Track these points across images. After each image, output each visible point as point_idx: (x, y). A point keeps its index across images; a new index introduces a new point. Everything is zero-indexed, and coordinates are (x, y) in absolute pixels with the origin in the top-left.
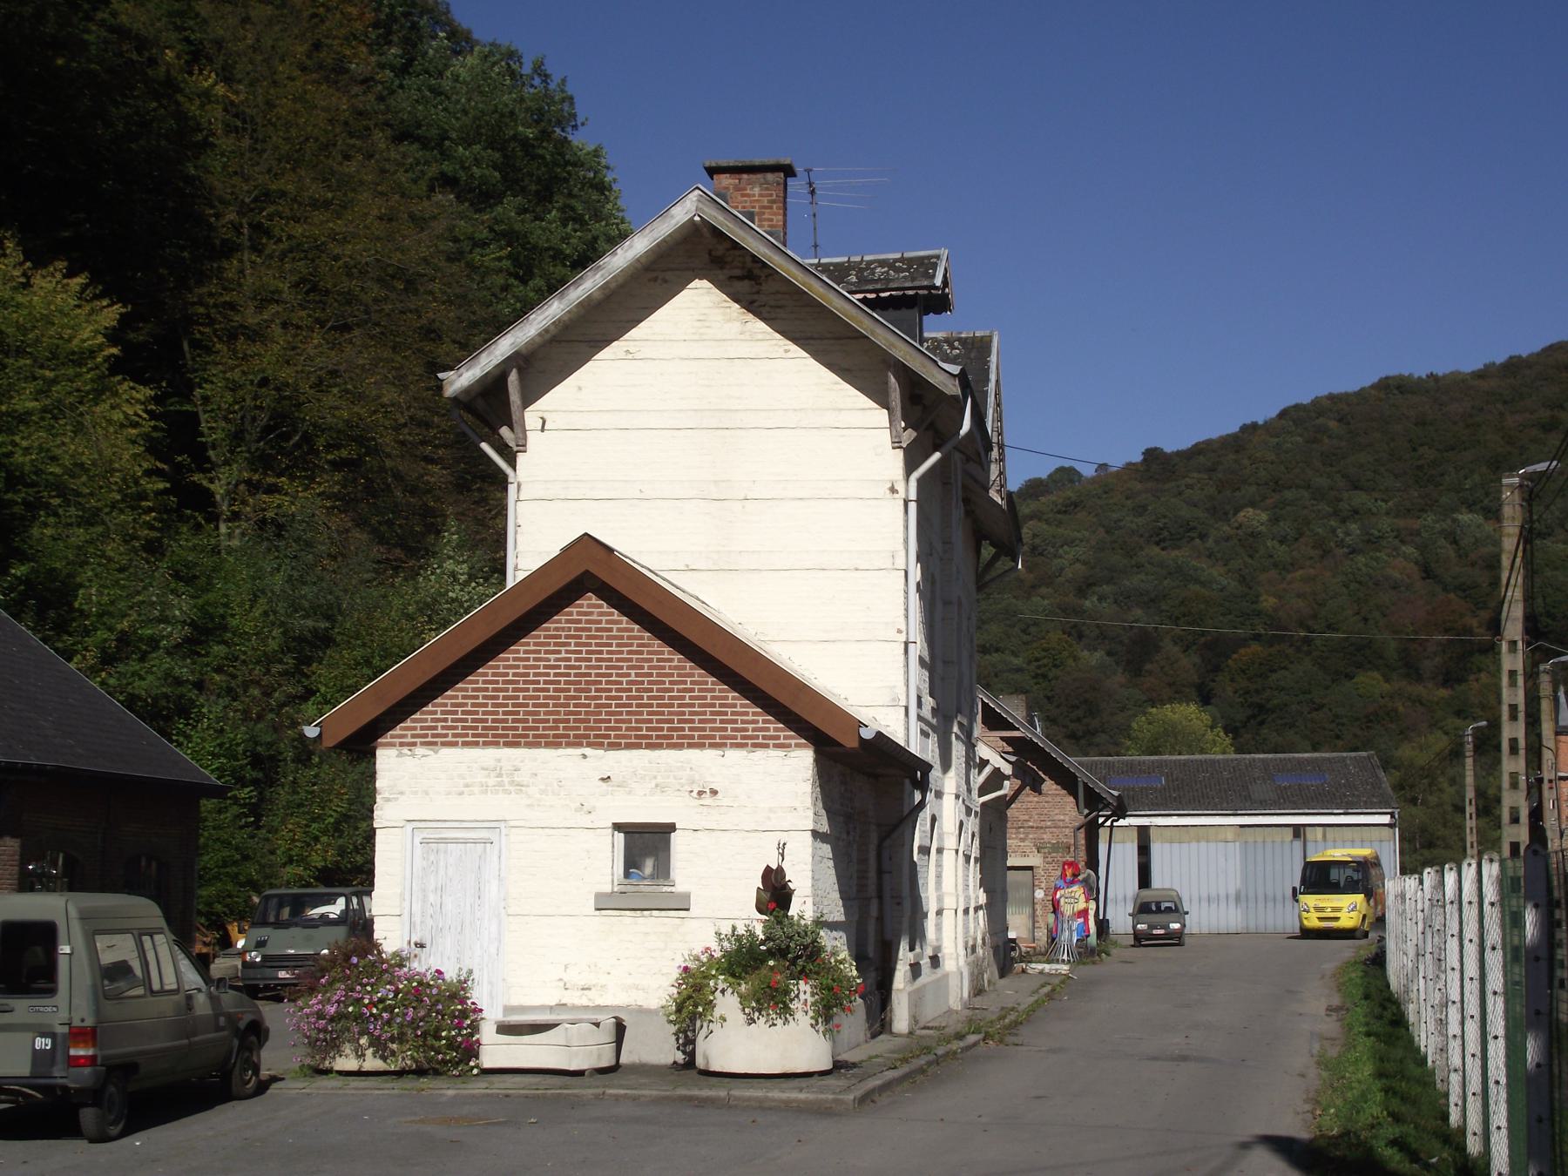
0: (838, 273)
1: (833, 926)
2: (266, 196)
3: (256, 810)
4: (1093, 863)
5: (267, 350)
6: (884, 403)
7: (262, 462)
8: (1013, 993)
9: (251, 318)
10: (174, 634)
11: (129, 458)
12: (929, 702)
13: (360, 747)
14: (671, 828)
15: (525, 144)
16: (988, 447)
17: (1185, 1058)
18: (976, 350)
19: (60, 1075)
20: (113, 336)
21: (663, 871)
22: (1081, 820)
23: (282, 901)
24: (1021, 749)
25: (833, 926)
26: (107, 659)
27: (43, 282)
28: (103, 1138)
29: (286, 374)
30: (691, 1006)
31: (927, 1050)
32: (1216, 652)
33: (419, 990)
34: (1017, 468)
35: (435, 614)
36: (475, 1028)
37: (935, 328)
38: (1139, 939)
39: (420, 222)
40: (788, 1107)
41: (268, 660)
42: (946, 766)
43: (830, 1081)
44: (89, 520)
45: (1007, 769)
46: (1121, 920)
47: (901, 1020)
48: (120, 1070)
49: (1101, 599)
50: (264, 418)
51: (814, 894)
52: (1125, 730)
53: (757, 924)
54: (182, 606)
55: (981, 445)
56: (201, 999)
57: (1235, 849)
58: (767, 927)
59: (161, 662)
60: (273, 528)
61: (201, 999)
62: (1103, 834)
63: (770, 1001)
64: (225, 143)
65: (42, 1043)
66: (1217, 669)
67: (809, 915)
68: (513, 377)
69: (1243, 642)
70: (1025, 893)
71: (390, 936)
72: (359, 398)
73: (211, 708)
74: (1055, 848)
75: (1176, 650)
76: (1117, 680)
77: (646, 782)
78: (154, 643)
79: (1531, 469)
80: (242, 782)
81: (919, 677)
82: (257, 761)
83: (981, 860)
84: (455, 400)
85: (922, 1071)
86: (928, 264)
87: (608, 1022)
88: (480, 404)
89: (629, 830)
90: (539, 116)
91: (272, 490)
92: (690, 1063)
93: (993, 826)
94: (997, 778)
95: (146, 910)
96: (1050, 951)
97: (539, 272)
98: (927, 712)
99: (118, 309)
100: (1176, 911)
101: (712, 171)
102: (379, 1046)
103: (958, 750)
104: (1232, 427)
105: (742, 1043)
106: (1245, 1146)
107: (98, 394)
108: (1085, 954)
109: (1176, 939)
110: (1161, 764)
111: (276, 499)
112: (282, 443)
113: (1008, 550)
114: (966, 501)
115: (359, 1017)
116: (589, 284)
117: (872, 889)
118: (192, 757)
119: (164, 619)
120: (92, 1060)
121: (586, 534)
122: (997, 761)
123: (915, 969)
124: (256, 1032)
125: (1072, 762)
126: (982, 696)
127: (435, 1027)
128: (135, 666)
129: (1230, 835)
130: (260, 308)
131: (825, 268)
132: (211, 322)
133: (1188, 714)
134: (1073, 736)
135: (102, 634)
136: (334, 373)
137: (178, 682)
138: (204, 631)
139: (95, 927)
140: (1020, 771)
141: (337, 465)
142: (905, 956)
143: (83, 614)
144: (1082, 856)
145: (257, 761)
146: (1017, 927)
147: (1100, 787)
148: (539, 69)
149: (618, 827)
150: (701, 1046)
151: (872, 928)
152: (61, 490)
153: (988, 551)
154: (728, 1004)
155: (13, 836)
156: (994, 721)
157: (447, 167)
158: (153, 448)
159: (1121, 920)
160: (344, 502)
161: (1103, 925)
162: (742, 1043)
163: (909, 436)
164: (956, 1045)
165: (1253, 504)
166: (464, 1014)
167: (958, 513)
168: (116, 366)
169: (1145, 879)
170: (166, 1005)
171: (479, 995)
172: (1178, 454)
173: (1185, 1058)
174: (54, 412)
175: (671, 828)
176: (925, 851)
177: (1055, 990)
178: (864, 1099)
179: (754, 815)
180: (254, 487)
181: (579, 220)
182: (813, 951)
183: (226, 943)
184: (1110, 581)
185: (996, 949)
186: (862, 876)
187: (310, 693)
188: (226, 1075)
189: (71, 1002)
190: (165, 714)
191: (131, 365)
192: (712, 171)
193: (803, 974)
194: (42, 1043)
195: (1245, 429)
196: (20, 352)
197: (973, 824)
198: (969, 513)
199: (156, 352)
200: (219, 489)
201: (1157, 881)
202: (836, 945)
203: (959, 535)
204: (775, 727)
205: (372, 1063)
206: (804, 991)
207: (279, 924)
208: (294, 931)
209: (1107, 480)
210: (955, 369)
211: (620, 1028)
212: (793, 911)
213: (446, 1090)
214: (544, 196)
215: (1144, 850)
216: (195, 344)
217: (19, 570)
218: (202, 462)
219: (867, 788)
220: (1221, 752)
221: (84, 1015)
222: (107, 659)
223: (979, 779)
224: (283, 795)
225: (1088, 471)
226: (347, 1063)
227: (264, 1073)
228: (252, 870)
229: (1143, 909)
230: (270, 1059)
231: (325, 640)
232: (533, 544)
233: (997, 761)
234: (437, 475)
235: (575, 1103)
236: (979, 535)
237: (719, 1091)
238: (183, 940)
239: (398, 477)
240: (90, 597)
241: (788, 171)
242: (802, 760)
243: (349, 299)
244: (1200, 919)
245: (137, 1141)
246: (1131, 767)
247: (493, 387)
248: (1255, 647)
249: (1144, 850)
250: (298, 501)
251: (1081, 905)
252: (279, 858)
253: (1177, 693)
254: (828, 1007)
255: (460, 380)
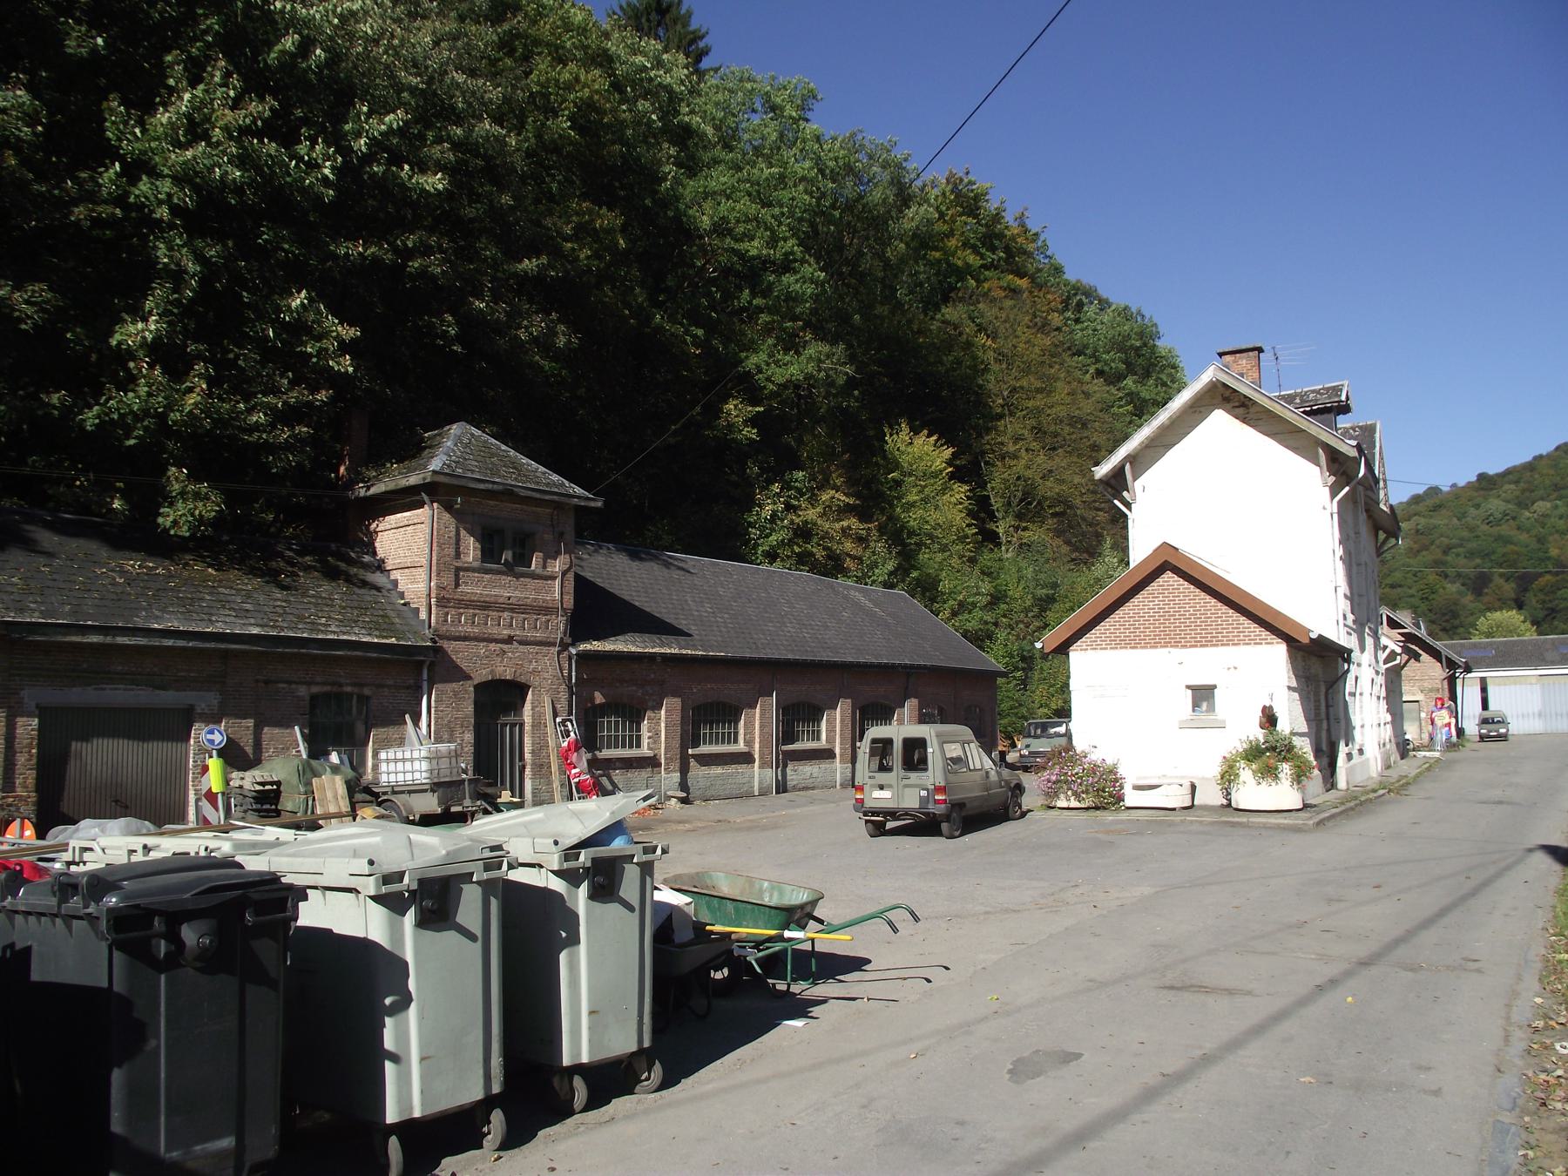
0: (1289, 399)
1: (1302, 735)
2: (1014, 390)
3: (1024, 683)
4: (1453, 697)
5: (1019, 461)
6: (1318, 465)
7: (1020, 516)
8: (1407, 768)
9: (1011, 448)
10: (985, 600)
11: (958, 518)
12: (1351, 617)
13: (1063, 649)
14: (1215, 687)
15: (1137, 349)
16: (1377, 481)
17: (1500, 802)
18: (1369, 431)
19: (932, 808)
20: (949, 463)
21: (1211, 709)
22: (1445, 675)
23: (1037, 726)
24: (1409, 638)
25: (1302, 735)
26: (954, 614)
27: (920, 440)
28: (952, 837)
29: (1028, 473)
30: (1228, 777)
31: (1356, 798)
32: (1525, 582)
33: (1094, 769)
34: (1395, 494)
35: (1099, 582)
36: (1122, 787)
37: (1343, 422)
38: (1482, 738)
39: (1087, 395)
40: (1279, 827)
41: (1026, 610)
42: (1363, 649)
43: (1300, 814)
44: (944, 548)
45: (1399, 650)
46: (1471, 728)
47: (1342, 782)
48: (958, 806)
49: (1458, 555)
50: (1019, 494)
51: (1292, 718)
52: (1474, 626)
53: (1259, 735)
54: (986, 587)
55: (1372, 482)
56: (993, 773)
57: (1538, 687)
58: (1265, 736)
59: (977, 613)
60: (1024, 547)
61: (993, 773)
62: (1459, 682)
63: (1269, 773)
64: (995, 367)
65: (924, 793)
66: (1526, 590)
67: (1287, 732)
68: (1128, 467)
69: (1541, 575)
70: (1415, 715)
71: (1079, 744)
72: (1063, 481)
73: (1001, 635)
74: (1431, 690)
75: (1501, 581)
76: (1468, 599)
77: (1203, 664)
78: (974, 605)
79: (596, 646)
80: (1017, 669)
81: (1345, 605)
82: (1023, 659)
83: (1387, 698)
84: (1100, 480)
85: (1352, 809)
86: (1337, 390)
87: (1187, 785)
88: (1113, 482)
89: (1195, 689)
90: (1141, 335)
91: (1025, 529)
92: (1229, 805)
93: (1393, 679)
94: (1393, 655)
95: (965, 732)
96: (1430, 745)
97: (1142, 409)
98: (1350, 621)
99: (951, 450)
100: (1502, 722)
101: (1221, 355)
102: (1077, 795)
103: (1369, 641)
104: (1528, 458)
105: (1253, 793)
106: (1530, 850)
107: (944, 491)
108: (1450, 746)
109: (1503, 738)
110: (1491, 644)
111: (1026, 534)
112: (1029, 507)
113: (1394, 533)
114: (1367, 511)
115: (1066, 782)
116: (1163, 417)
117: (1323, 715)
118: (992, 660)
119: (978, 594)
120: (944, 801)
121: (1165, 544)
122: (1393, 646)
123: (1349, 756)
124: (1019, 789)
125: (1438, 645)
126: (1385, 612)
127: (1104, 791)
128: (967, 616)
129: (1534, 680)
130: (1015, 443)
131: (1283, 398)
132: (994, 452)
133: (1512, 616)
134: (1444, 630)
135: (951, 602)
136: (1051, 471)
137: (986, 623)
138: (996, 599)
139: (943, 740)
140: (1406, 650)
141: (1055, 515)
142: (1343, 750)
143: (943, 594)
144: (1446, 695)
145: (1023, 659)
146: (1411, 733)
147: (1455, 657)
148: (1139, 313)
149: (1188, 687)
150: (1234, 796)
151: (1324, 735)
152: (931, 537)
153: (1382, 536)
154: (1246, 774)
155: (674, 696)
156: (1393, 624)
157: (1098, 366)
158: (970, 514)
159: (1471, 728)
160: (1058, 533)
161: (1460, 732)
162: (1253, 793)
163: (1333, 479)
164: (1372, 796)
165: (1542, 499)
166: (1116, 780)
167: (1363, 516)
168: (952, 476)
169: (1485, 706)
170: (977, 776)
171: (1122, 771)
172: (1497, 475)
173: (1500, 802)
174: (925, 500)
175: (1215, 687)
176: (1353, 694)
177: (1431, 766)
178: (1318, 824)
179: (1260, 678)
180: (1017, 528)
181: (1164, 384)
182: (1290, 748)
183: (1014, 745)
184: (1461, 546)
185: (1398, 745)
186: (1317, 708)
187: (1046, 626)
188: (1006, 808)
189: (934, 774)
190: (980, 639)
191: (958, 475)
192: (1221, 355)
193: (1285, 759)
194: (924, 793)
195: (1535, 458)
196: (910, 475)
197: (1380, 680)
198: (1370, 517)
199: (968, 470)
200: (1001, 531)
201: (1492, 706)
202: (1304, 746)
203: (1364, 529)
204: (1265, 634)
205: (1074, 803)
206: (1286, 769)
207: (1036, 737)
208: (1043, 740)
209: (1457, 492)
210: (1354, 443)
211: (1193, 787)
212: (1279, 728)
213: (1108, 817)
214: (1147, 374)
215: (1484, 690)
216: (987, 463)
217: (914, 574)
218: (992, 516)
219: (1318, 665)
220: (1530, 635)
221: (941, 782)
222: (954, 614)
223: (1382, 656)
224: (1036, 675)
225: (1446, 489)
226: (1062, 803)
227: (1024, 808)
228: (1024, 711)
229: (1485, 721)
230: (1027, 801)
231: (1051, 600)
232: (1141, 548)
233: (1393, 646)
234: (1102, 516)
235: (1171, 824)
236: (1376, 528)
237: (1243, 819)
238: (988, 746)
239: (1084, 519)
240: (945, 585)
241: (1260, 350)
242: (1281, 649)
243: (1056, 435)
244: (1516, 727)
245: (967, 838)
246: (1475, 646)
247: (1119, 473)
248: (1548, 577)
249: (1484, 690)
250: (1035, 534)
251: (1447, 720)
252: (1037, 705)
253: (1502, 604)
254: (1299, 776)
255: (1102, 471)
